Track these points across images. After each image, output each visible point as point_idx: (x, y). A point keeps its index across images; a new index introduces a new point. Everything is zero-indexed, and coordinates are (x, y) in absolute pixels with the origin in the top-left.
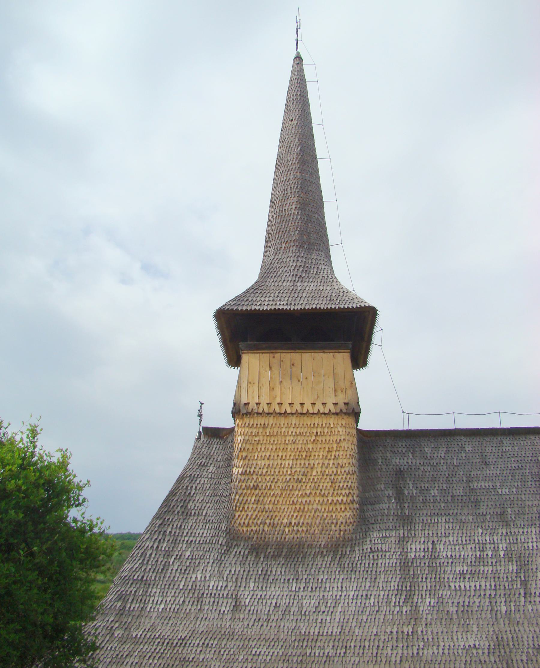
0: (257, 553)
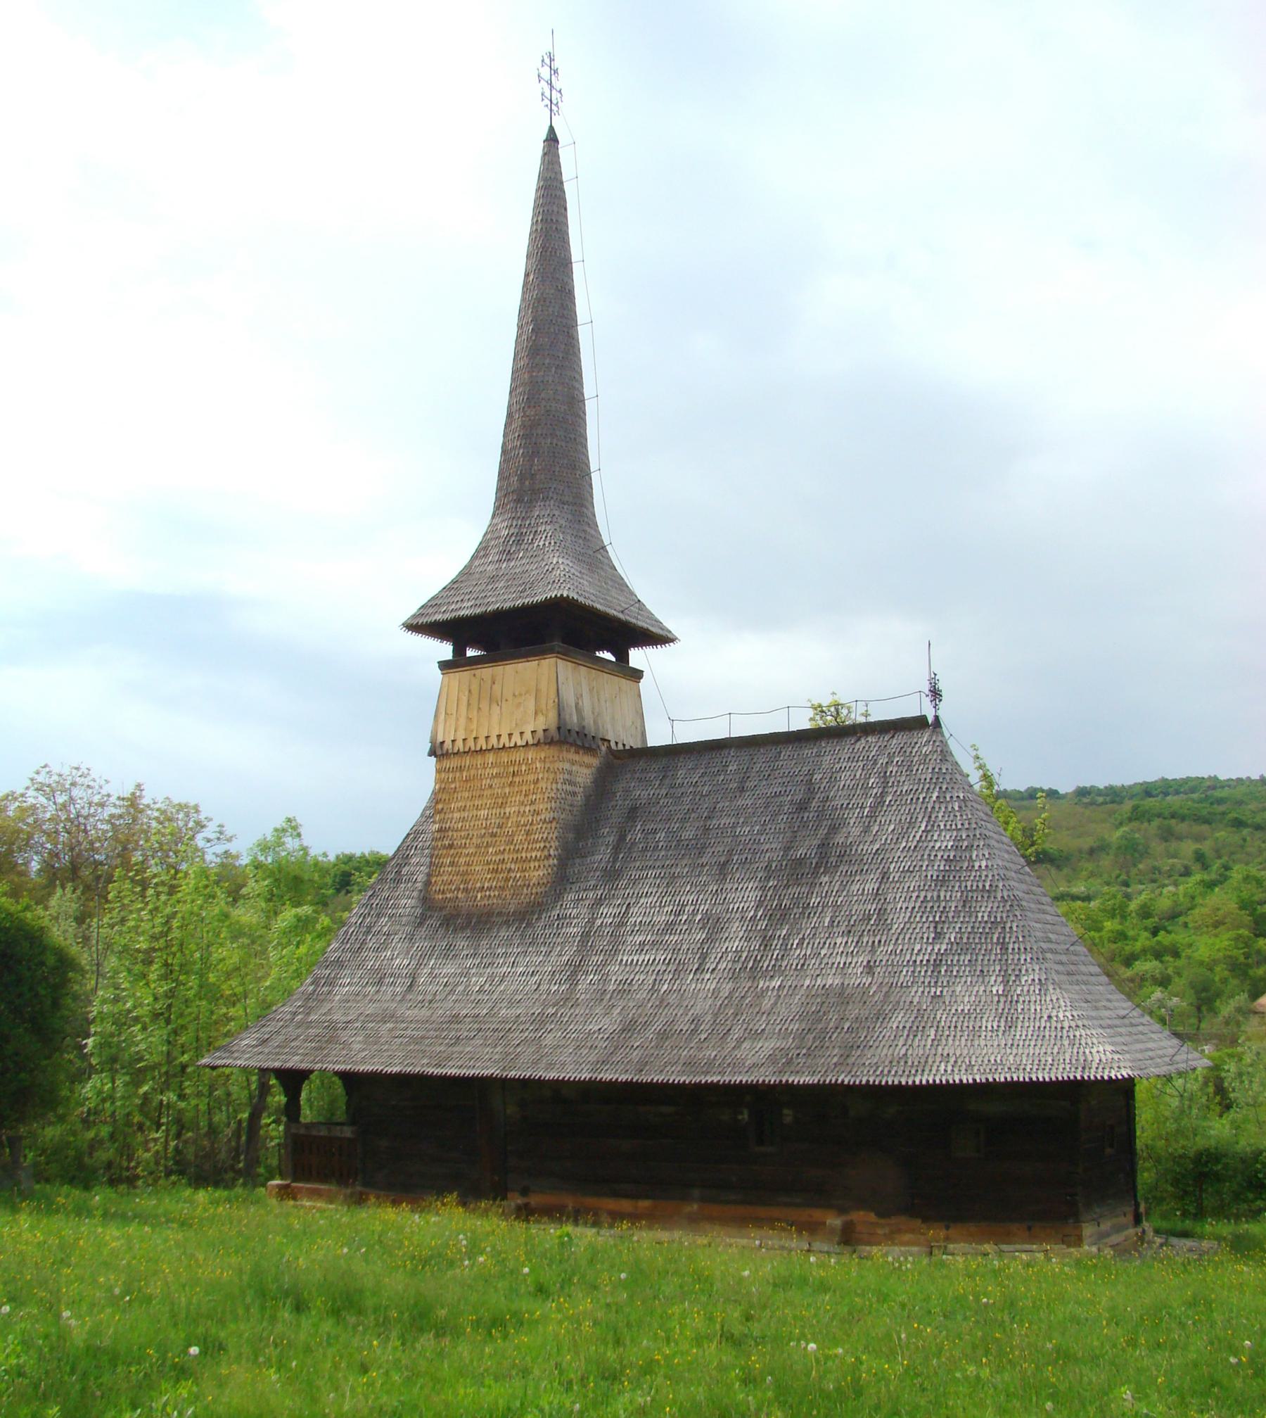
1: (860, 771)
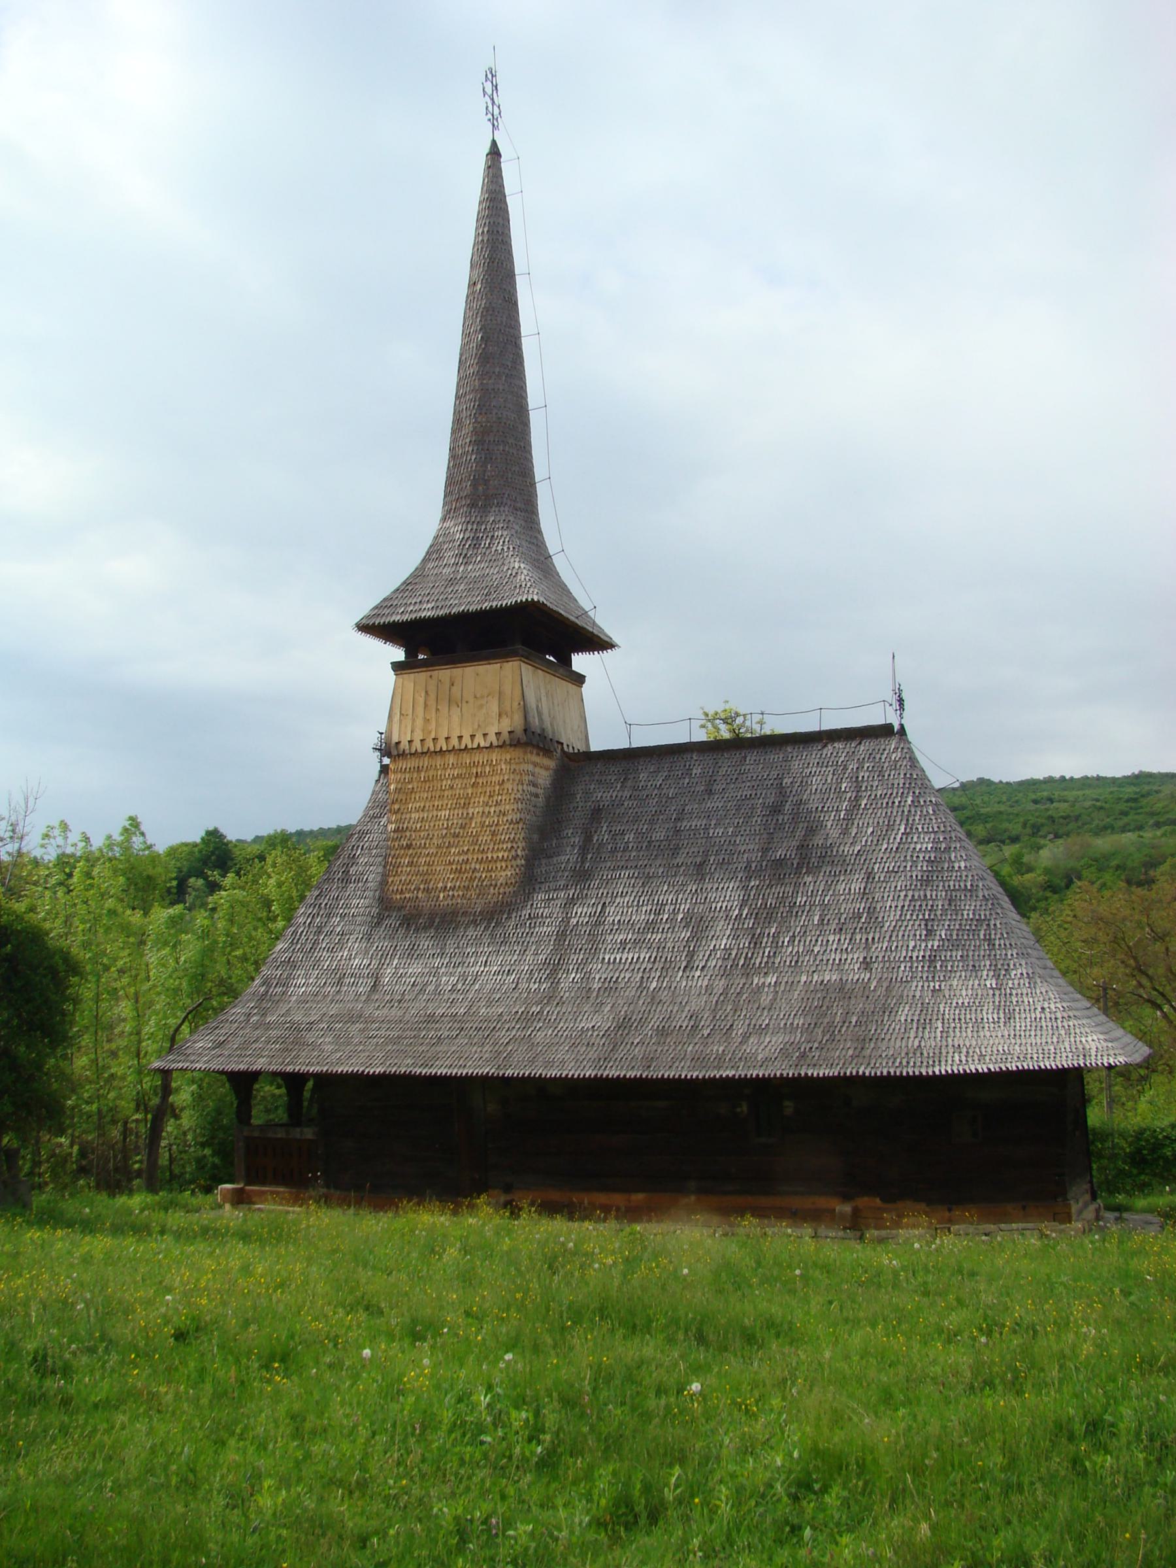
0: (408, 924)
1: (831, 776)
